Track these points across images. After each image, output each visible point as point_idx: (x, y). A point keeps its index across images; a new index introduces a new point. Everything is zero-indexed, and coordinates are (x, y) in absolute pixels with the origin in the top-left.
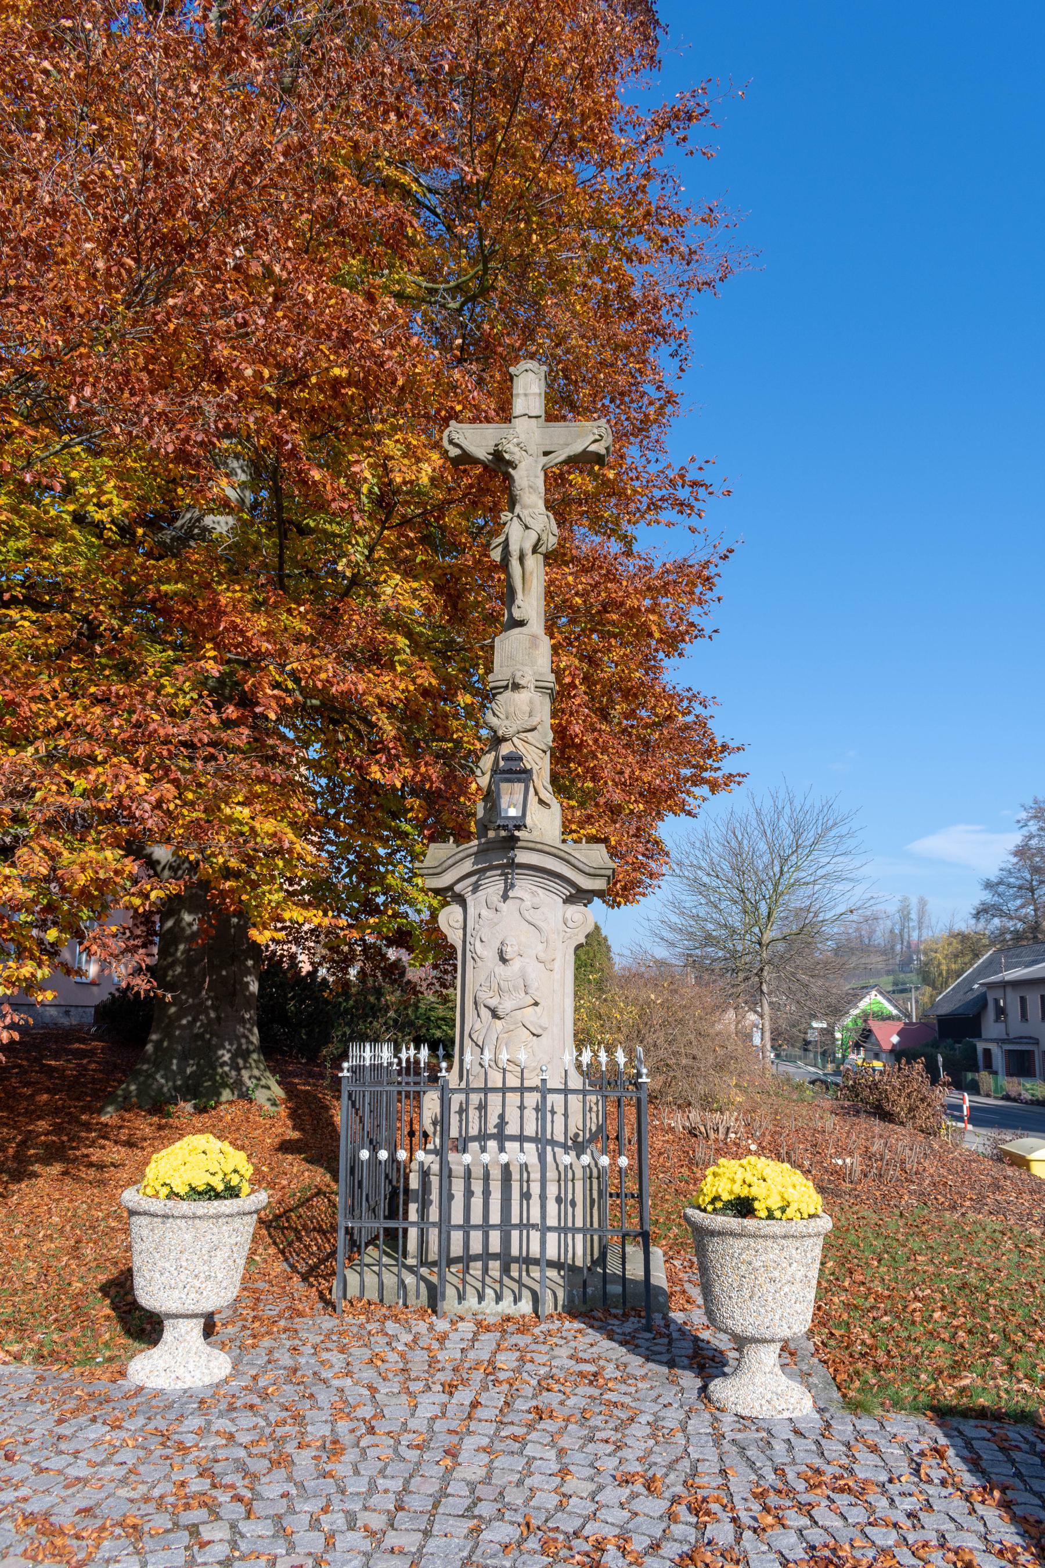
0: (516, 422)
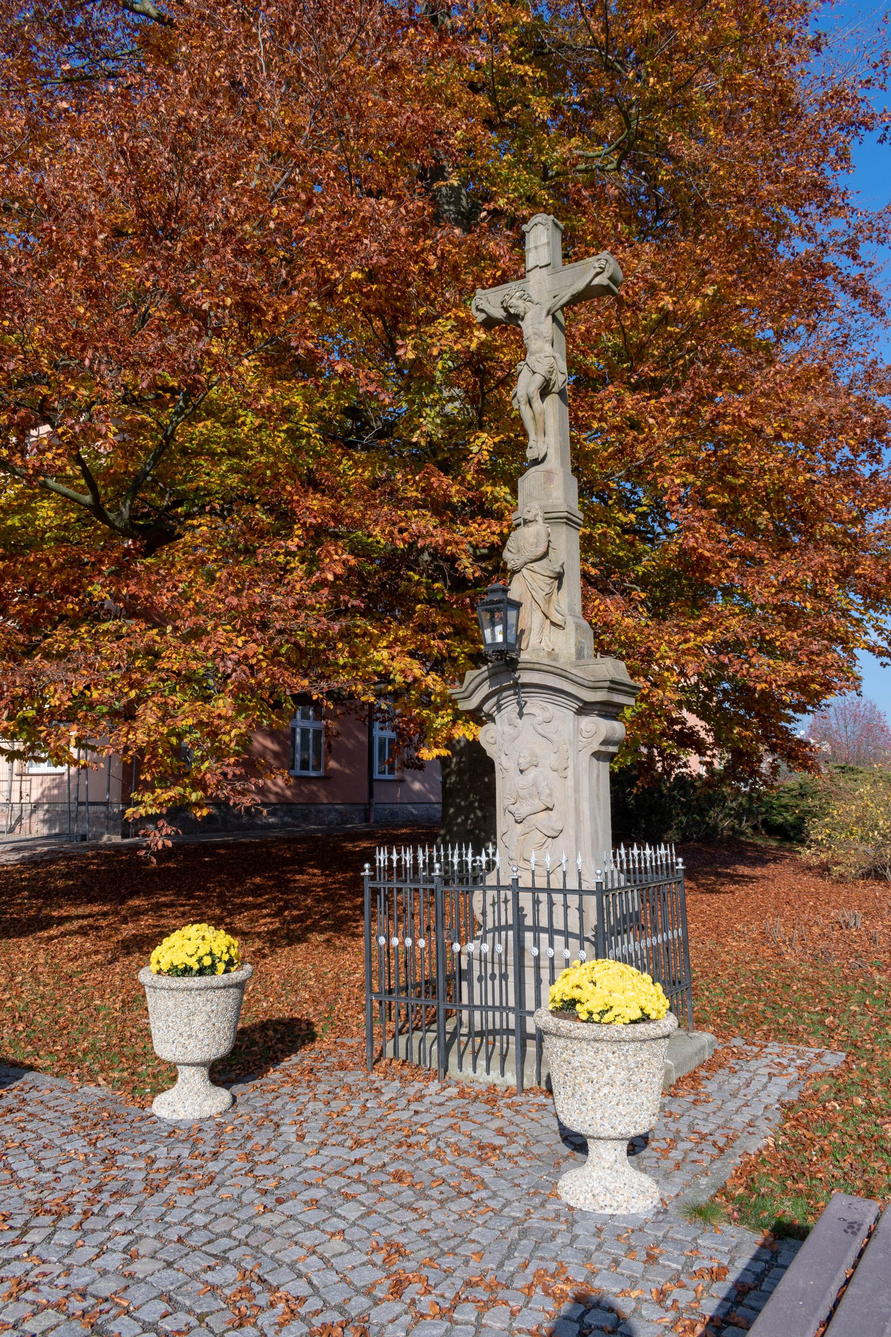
0: (530, 275)
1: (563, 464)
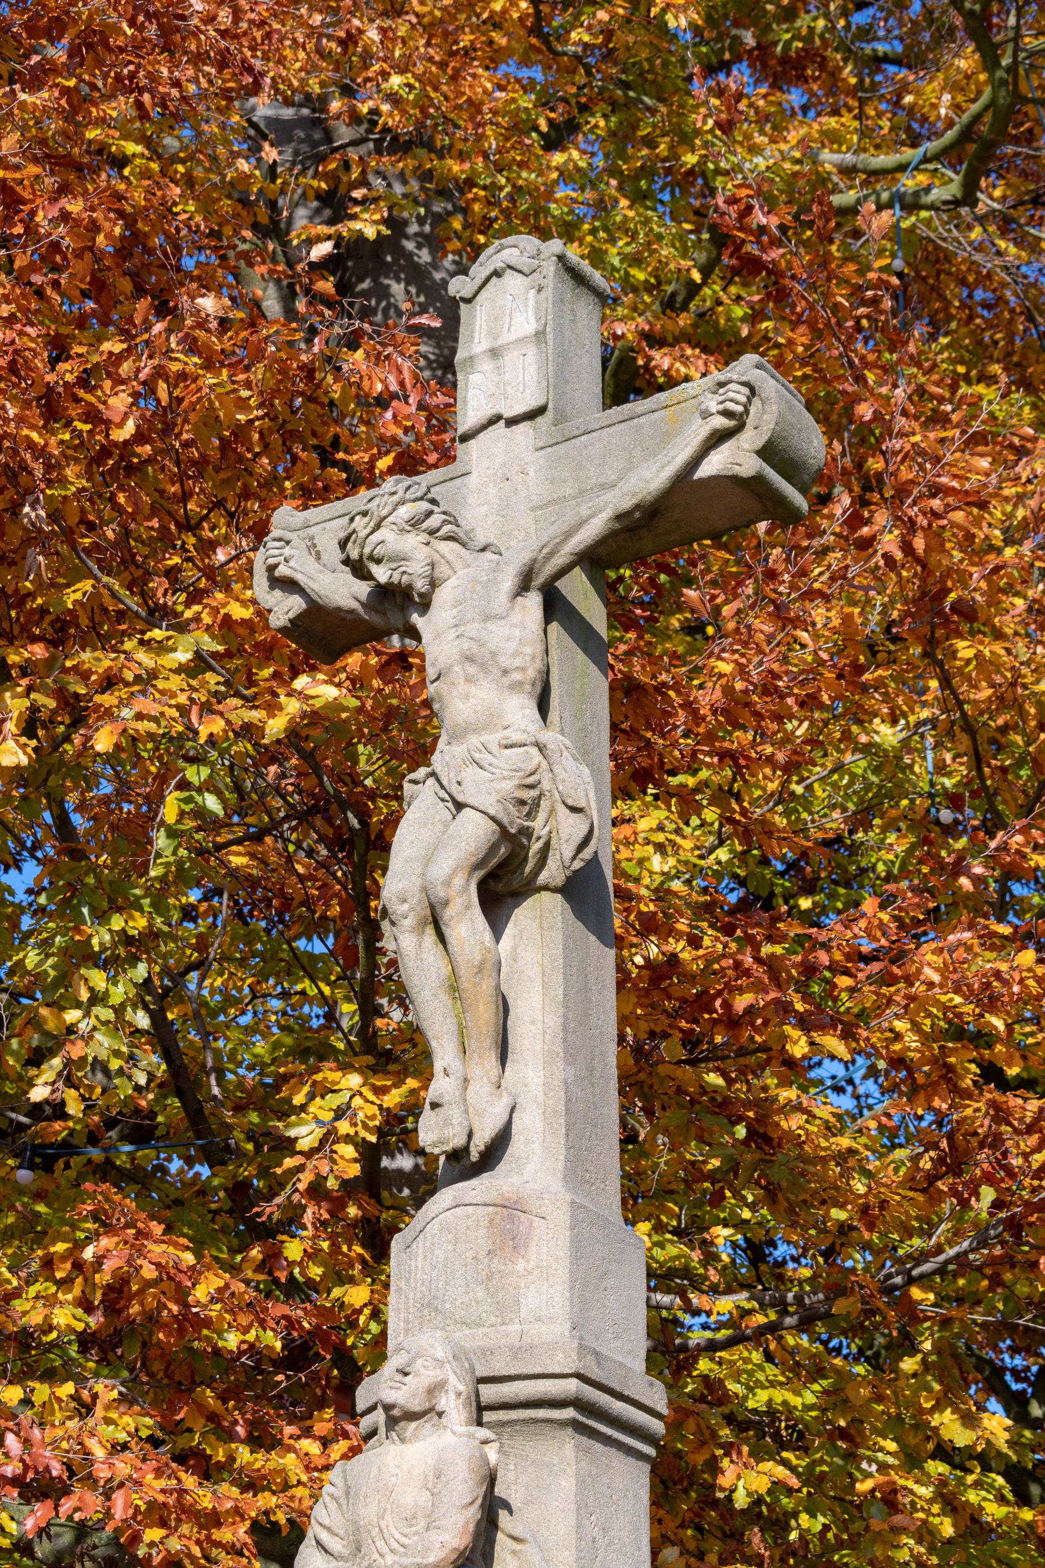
0: (471, 453)
1: (576, 1172)
